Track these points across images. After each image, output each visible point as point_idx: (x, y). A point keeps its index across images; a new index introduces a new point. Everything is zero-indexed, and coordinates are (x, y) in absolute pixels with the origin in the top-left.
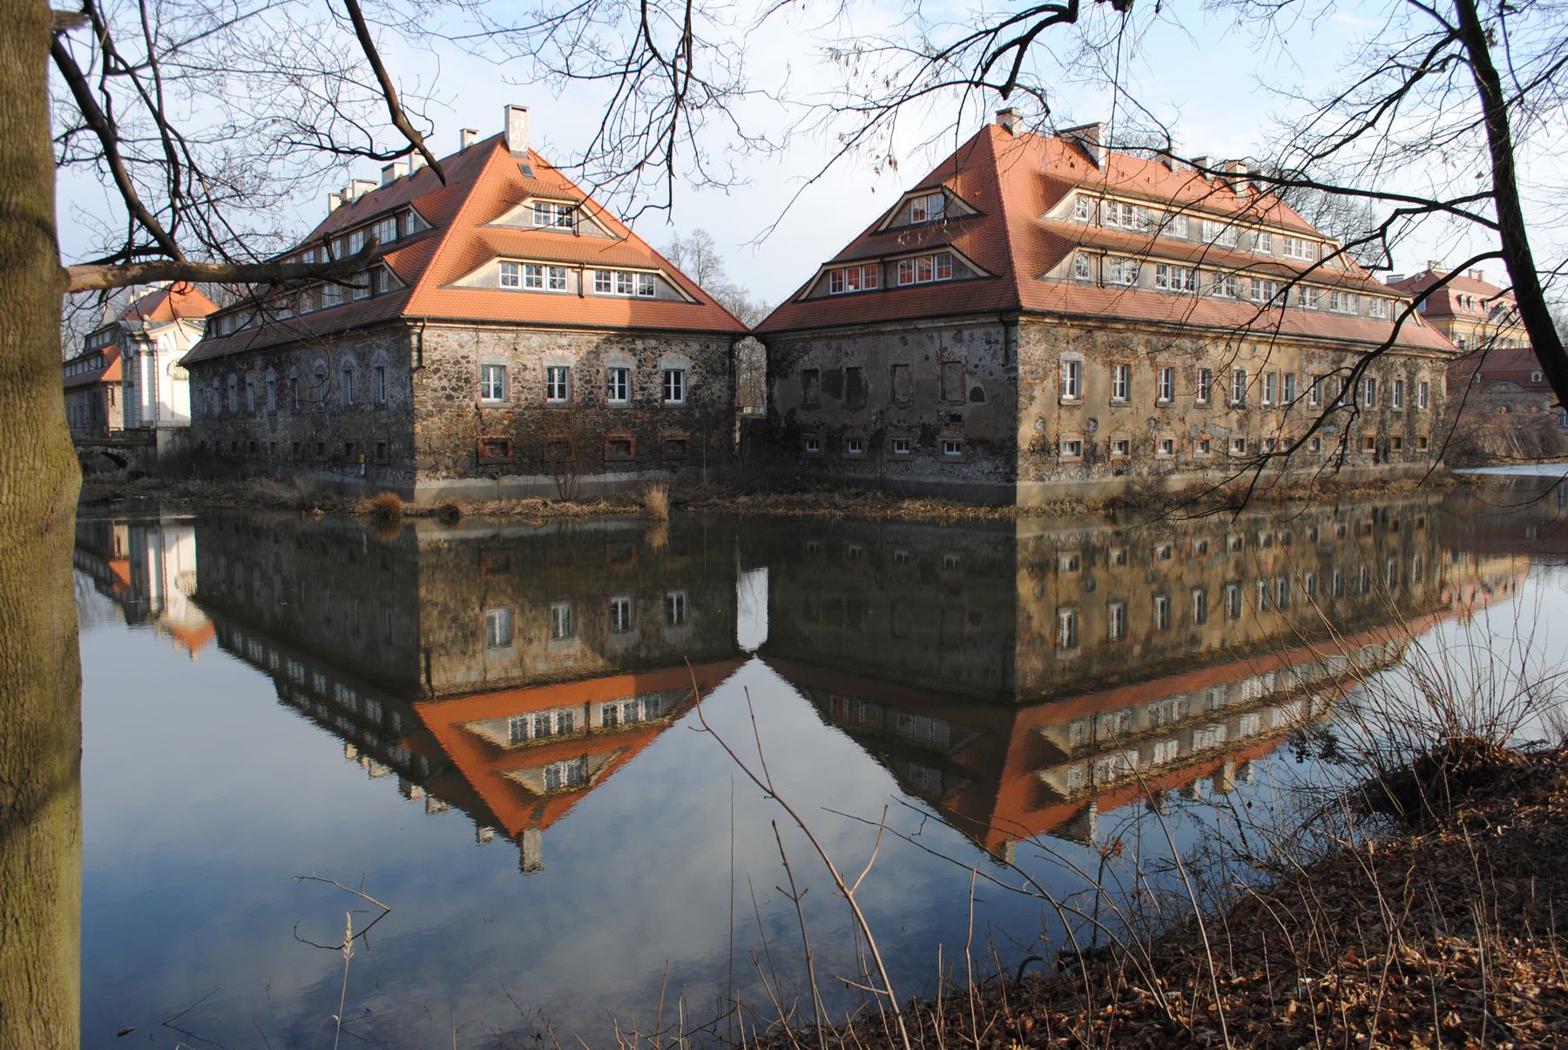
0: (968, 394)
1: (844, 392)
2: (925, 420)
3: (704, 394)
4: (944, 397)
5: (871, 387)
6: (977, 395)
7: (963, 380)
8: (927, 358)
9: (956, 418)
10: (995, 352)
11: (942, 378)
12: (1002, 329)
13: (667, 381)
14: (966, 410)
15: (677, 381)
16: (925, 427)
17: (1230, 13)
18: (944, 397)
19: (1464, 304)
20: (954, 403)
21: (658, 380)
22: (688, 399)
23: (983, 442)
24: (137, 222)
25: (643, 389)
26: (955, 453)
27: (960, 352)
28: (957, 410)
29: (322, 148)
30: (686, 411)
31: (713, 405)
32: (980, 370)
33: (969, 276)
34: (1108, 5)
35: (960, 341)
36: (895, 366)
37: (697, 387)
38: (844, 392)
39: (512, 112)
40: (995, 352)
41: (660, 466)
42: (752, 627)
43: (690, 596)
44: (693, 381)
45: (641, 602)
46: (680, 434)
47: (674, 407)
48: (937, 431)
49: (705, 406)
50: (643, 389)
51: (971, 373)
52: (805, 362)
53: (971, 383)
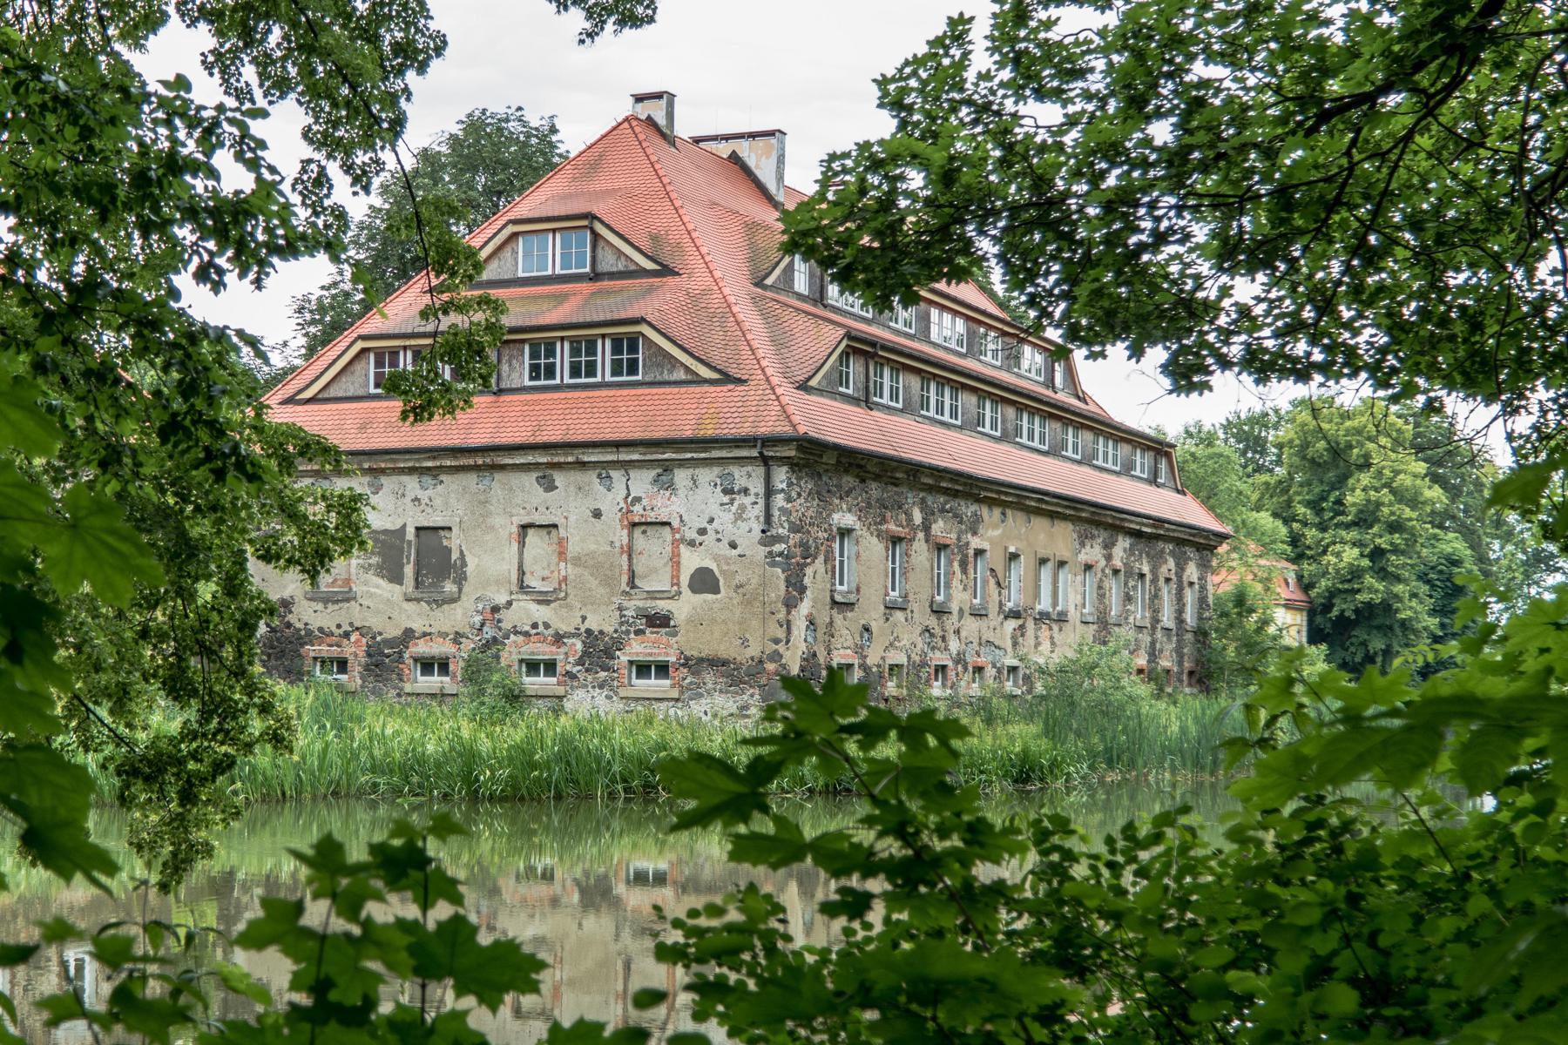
0: (685, 579)
1: (409, 570)
2: (593, 623)
4: (632, 583)
6: (704, 581)
8: (597, 514)
9: (659, 621)
10: (742, 508)
11: (630, 551)
12: (761, 470)
14: (684, 607)
17: (576, 19)
18: (632, 583)
20: (653, 596)
23: (716, 663)
24: (633, 267)
26: (542, 679)
27: (667, 506)
28: (662, 606)
32: (709, 538)
33: (680, 375)
35: (670, 486)
36: (525, 527)
38: (409, 570)
39: (663, 102)
40: (742, 508)
48: (619, 644)
51: (692, 543)
53: (691, 561)
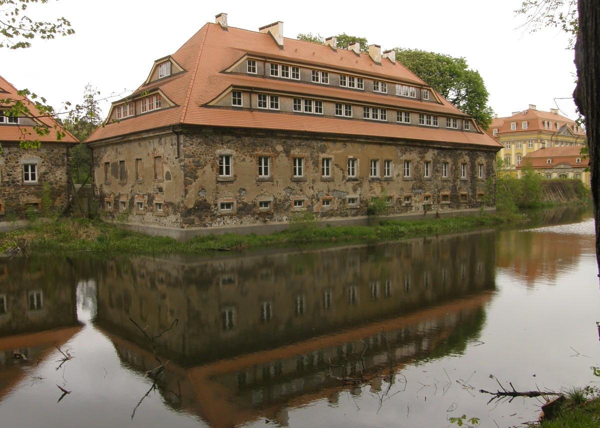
3: (51, 177)
5: (128, 171)
7: (163, 167)
13: (27, 170)
15: (33, 170)
16: (149, 195)
19: (546, 125)
21: (19, 170)
22: (39, 180)
25: (8, 175)
29: (557, 8)
30: (39, 186)
31: (56, 183)
34: (34, 1)
37: (46, 173)
41: (22, 218)
42: (85, 314)
43: (45, 293)
44: (43, 170)
45: (12, 298)
46: (33, 199)
47: (33, 185)
49: (51, 183)
50: (8, 175)
51: (166, 163)
52: (105, 159)
